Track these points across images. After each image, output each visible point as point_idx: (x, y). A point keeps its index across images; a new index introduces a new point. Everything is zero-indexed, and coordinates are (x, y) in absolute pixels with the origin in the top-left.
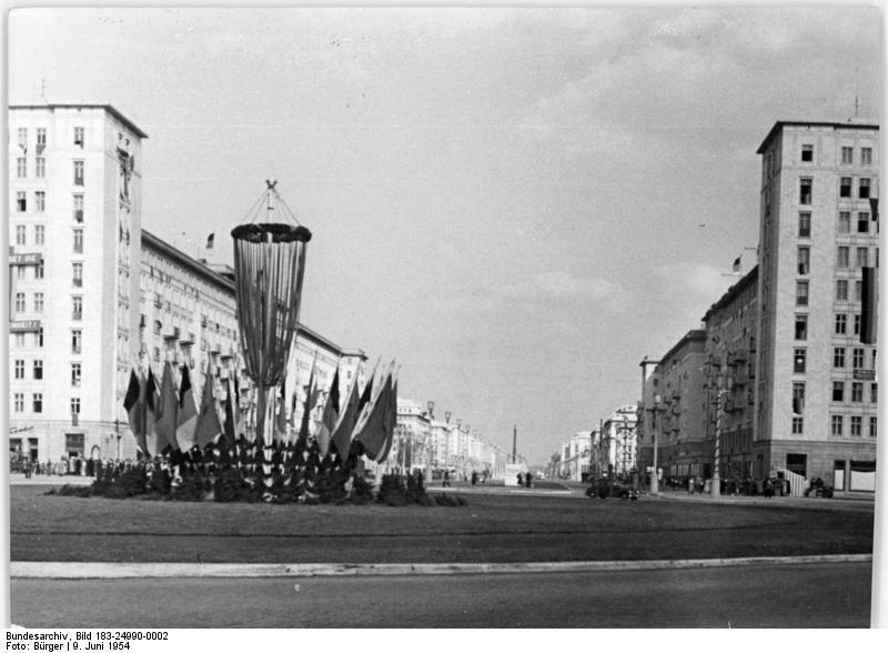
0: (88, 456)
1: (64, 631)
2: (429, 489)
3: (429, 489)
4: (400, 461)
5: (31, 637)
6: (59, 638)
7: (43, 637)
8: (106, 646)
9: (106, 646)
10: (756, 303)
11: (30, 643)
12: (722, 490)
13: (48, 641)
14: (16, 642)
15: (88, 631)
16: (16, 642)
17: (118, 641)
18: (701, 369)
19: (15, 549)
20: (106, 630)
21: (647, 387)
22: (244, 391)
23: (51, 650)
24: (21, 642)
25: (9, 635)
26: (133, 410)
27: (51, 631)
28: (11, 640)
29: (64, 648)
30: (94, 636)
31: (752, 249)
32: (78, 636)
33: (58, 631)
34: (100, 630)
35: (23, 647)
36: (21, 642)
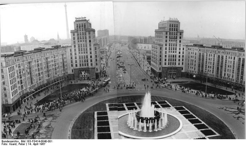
0: (45, 79)
4: (29, 111)
5: (9, 141)
6: (17, 142)
7: (12, 142)
8: (39, 144)
9: (39, 144)
10: (187, 133)
11: (8, 143)
12: (114, 134)
13: (12, 143)
14: (4, 143)
15: (24, 140)
16: (4, 143)
20: (29, 140)
21: (9, 105)
22: (176, 121)
24: (6, 143)
25: (2, 141)
26: (236, 138)
27: (14, 140)
29: (26, 144)
30: (26, 141)
32: (22, 141)
33: (16, 140)
34: (28, 140)
35: (7, 144)
36: (6, 143)
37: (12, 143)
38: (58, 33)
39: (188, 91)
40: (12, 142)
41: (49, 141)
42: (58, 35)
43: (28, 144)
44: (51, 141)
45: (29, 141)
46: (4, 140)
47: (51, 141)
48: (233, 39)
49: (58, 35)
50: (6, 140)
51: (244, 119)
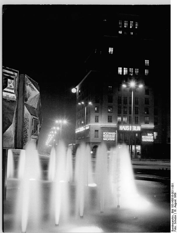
1: (171, 216)
2: (151, 126)
3: (151, 126)
5: (173, 225)
6: (173, 217)
7: (173, 222)
11: (174, 225)
14: (174, 229)
15: (171, 210)
16: (174, 229)
17: (174, 196)
18: (99, 104)
19: (169, 143)
20: (171, 205)
23: (176, 204)
24: (174, 227)
25: (172, 231)
28: (174, 230)
29: (176, 215)
30: (173, 208)
31: (137, 128)
32: (173, 212)
33: (171, 218)
34: (171, 207)
35: (176, 227)
36: (174, 227)
37: (174, 222)
38: (94, 162)
39: (106, 133)
40: (173, 222)
41: (172, 186)
42: (94, 156)
43: (175, 213)
44: (173, 184)
45: (172, 206)
46: (171, 229)
47: (173, 184)
48: (86, 227)
49: (94, 156)
50: (171, 227)
51: (137, 171)
